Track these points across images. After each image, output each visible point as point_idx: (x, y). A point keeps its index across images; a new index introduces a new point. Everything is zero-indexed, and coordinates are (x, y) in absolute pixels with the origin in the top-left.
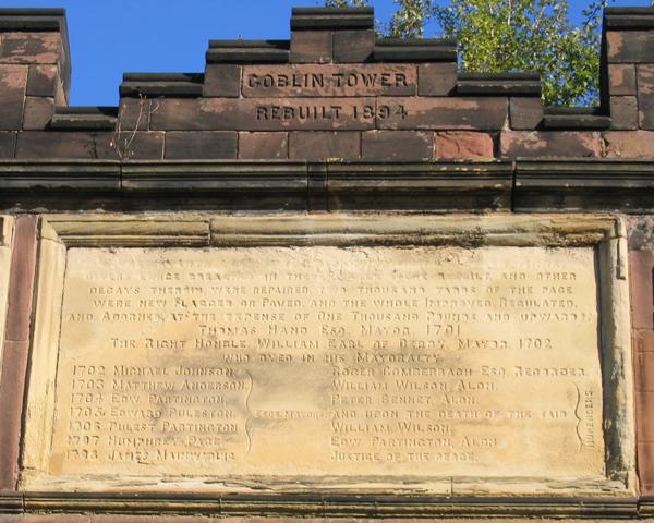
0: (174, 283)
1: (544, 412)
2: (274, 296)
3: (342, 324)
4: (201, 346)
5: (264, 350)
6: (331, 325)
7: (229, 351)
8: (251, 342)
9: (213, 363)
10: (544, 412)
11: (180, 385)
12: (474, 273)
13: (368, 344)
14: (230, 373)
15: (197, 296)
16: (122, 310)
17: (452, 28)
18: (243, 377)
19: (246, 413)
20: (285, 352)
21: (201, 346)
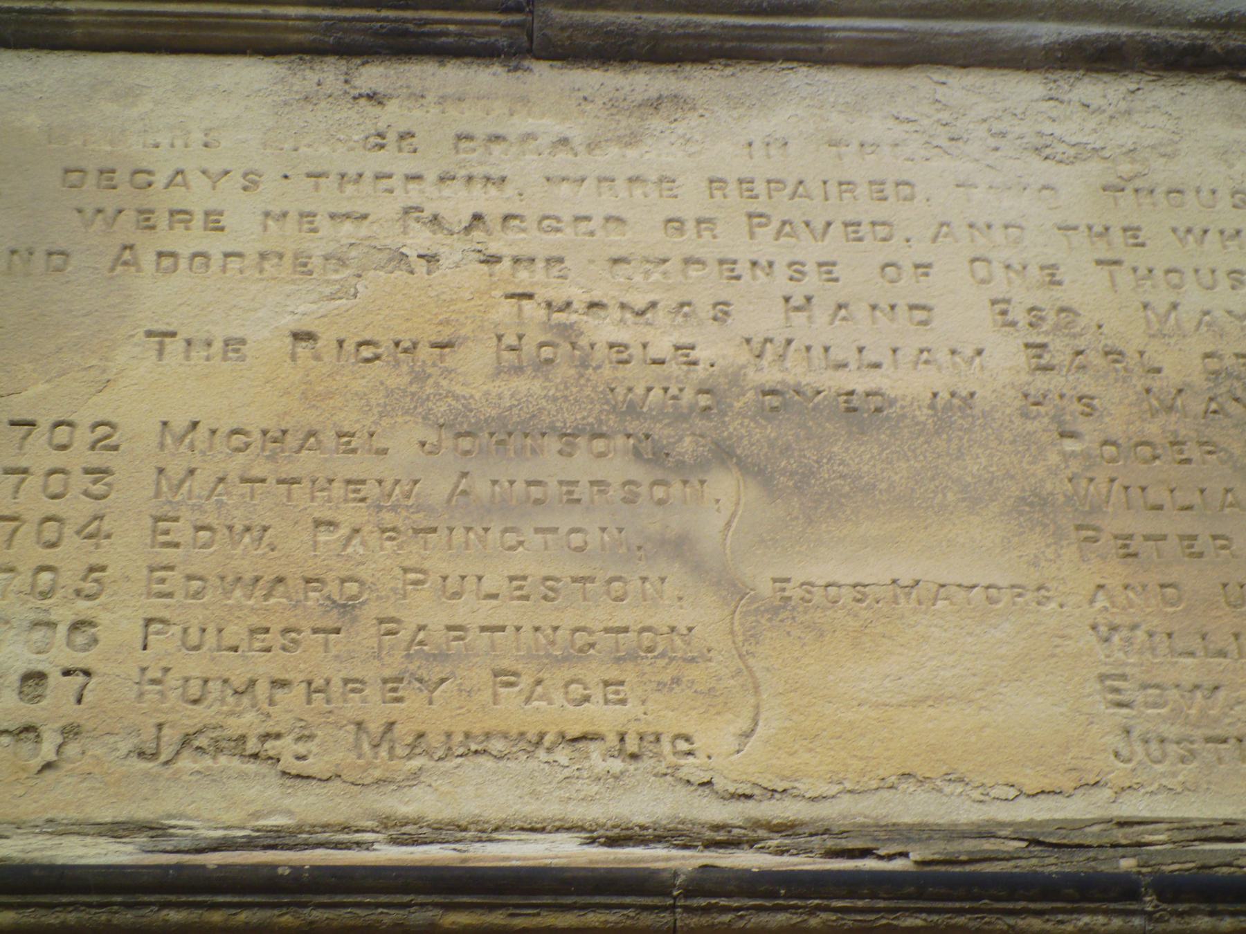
0: (397, 162)
1: (620, 362)
2: (782, 207)
3: (1063, 296)
4: (513, 359)
5: (770, 375)
6: (1023, 298)
7: (637, 376)
8: (716, 349)
9: (570, 418)
10: (620, 362)
11: (437, 487)
12: (931, 271)
13: (1181, 363)
14: (653, 454)
15: (490, 202)
16: (215, 245)
17: (394, 508)
18: (702, 465)
19: (734, 590)
20: (860, 382)
21: (513, 359)
